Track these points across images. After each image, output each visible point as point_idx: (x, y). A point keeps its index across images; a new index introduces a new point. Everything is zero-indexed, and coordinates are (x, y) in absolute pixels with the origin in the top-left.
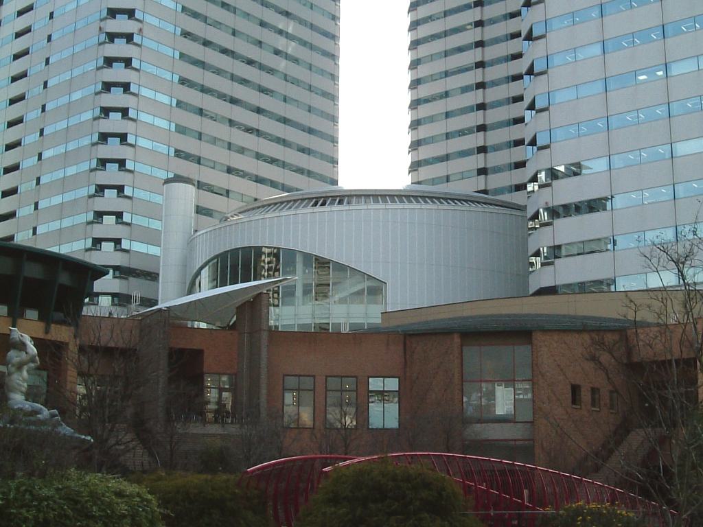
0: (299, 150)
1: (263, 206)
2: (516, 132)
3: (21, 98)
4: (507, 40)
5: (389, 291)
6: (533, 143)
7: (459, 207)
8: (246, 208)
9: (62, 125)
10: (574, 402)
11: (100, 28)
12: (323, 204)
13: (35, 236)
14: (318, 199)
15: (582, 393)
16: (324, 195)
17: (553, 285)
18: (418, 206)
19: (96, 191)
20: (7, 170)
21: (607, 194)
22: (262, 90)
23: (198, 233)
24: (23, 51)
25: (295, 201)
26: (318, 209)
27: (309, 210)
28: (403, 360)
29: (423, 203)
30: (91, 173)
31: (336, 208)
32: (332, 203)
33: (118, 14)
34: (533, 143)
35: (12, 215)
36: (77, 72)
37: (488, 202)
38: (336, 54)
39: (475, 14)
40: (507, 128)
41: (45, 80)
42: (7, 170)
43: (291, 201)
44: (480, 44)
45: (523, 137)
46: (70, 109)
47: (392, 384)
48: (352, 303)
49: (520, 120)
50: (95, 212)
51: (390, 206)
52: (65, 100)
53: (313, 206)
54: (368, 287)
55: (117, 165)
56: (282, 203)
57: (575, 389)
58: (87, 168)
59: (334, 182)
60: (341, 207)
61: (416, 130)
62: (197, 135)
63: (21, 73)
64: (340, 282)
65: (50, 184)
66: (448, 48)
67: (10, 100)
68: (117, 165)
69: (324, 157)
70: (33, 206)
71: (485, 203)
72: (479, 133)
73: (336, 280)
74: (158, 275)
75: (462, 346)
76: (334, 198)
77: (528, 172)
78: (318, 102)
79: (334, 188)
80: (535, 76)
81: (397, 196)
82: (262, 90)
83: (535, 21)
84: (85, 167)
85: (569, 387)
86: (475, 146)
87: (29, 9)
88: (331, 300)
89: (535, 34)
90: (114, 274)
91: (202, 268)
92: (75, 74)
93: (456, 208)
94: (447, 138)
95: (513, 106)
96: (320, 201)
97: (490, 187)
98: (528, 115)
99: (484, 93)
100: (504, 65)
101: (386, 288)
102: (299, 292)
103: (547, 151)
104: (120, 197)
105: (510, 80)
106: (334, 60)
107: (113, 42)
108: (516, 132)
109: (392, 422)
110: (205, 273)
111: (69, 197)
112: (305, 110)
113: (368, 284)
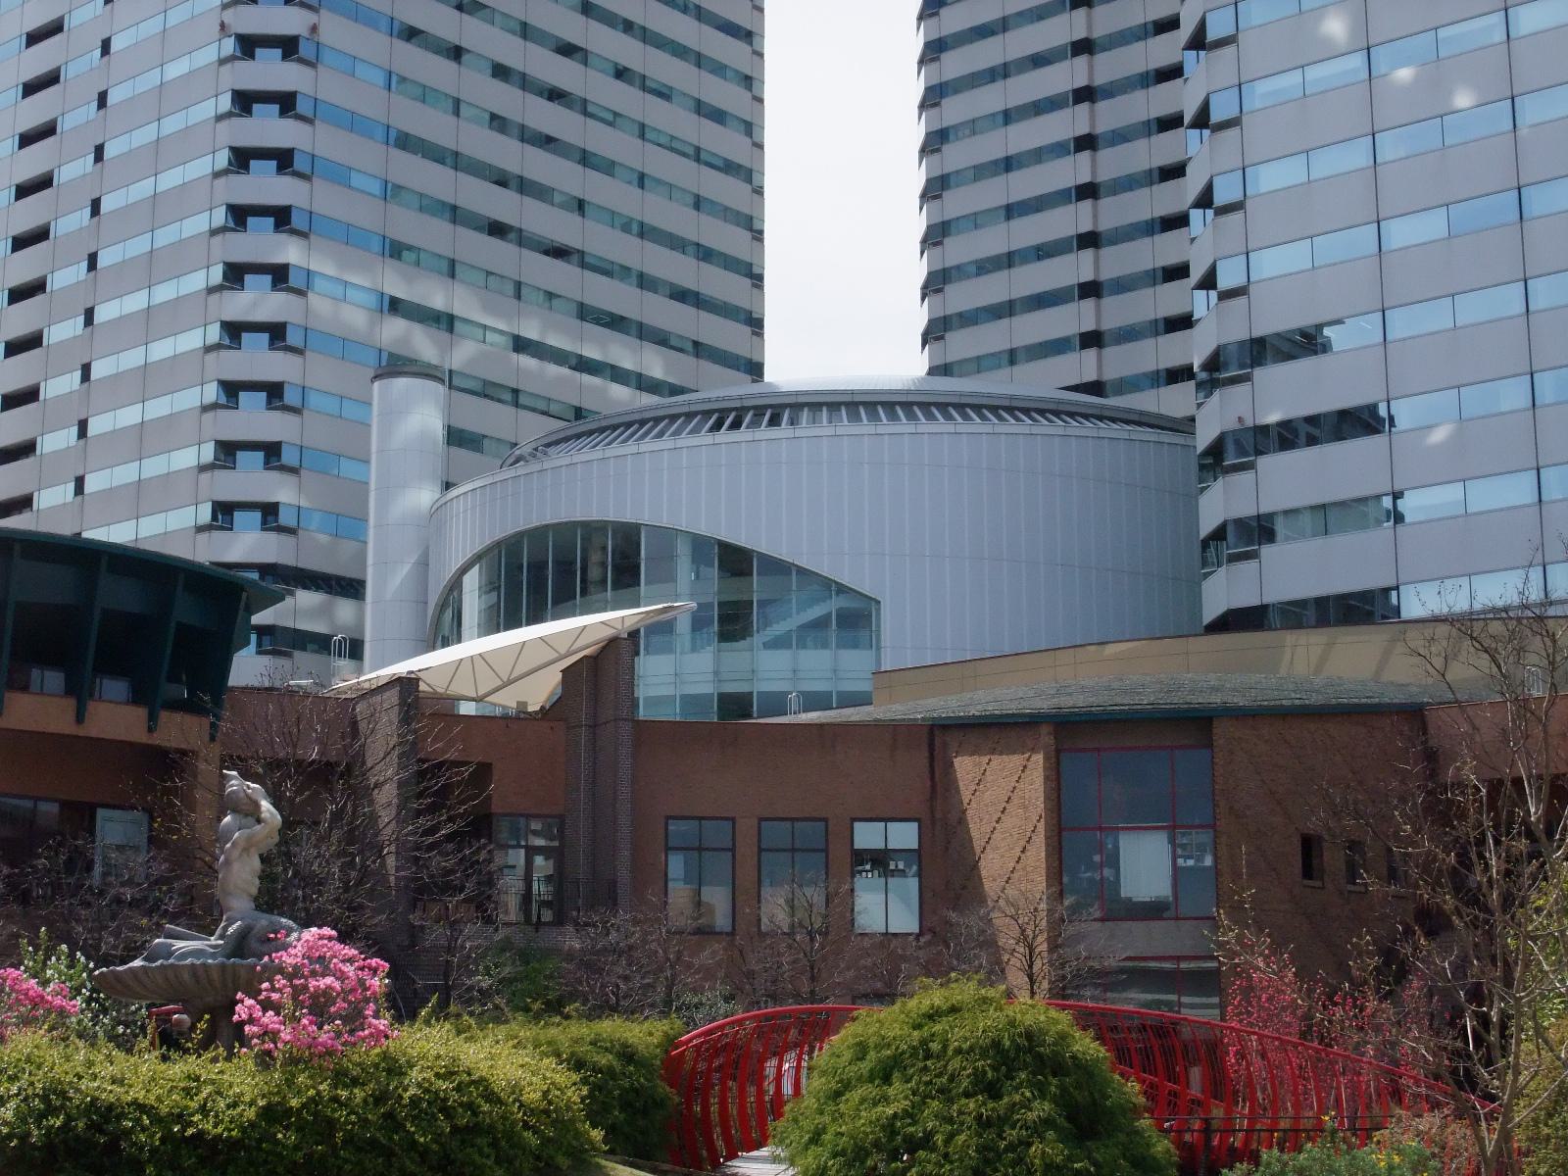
0: (672, 297)
1: (602, 430)
2: (1162, 100)
3: (51, 79)
4: (1152, 184)
5: (888, 622)
6: (1202, 120)
7: (1043, 427)
8: (562, 435)
9: (145, 135)
10: (1308, 872)
11: (223, 26)
12: (736, 425)
13: (79, 498)
14: (723, 413)
15: (1327, 855)
16: (738, 404)
17: (1255, 602)
18: (949, 427)
19: (214, 517)
20: (14, 348)
21: (1390, 582)
22: (585, 159)
23: (454, 492)
24: (46, 74)
25: (673, 418)
26: (724, 436)
27: (705, 438)
28: (929, 783)
29: (960, 420)
30: (216, 182)
31: (765, 433)
32: (755, 424)
33: (261, 46)
34: (1202, 120)
35: (26, 449)
36: (176, 17)
37: (1107, 413)
38: (754, 75)
39: (1071, 26)
40: (1147, 240)
41: (99, 142)
42: (14, 348)
43: (662, 418)
44: (1085, 95)
45: (1185, 259)
46: (162, 100)
47: (904, 836)
48: (804, 647)
49: (1174, 72)
50: (234, 150)
51: (885, 426)
52: (153, 79)
53: (711, 430)
54: (837, 610)
55: (264, 395)
56: (642, 423)
57: (1309, 845)
58: (198, 343)
59: (755, 369)
60: (774, 433)
61: (941, 295)
62: (444, 266)
63: (39, 176)
64: (775, 601)
65: (109, 493)
66: (1013, 103)
67: (15, 239)
68: (264, 395)
69: (730, 168)
70: (81, 319)
71: (1101, 418)
72: (1085, 352)
73: (765, 596)
74: (364, 582)
75: (1058, 751)
76: (759, 411)
77: (1191, 186)
78: (727, 239)
79: (756, 388)
80: (1213, 132)
81: (900, 404)
82: (585, 159)
83: (1218, 171)
84: (196, 281)
85: (1296, 843)
86: (1071, 232)
87: (55, 28)
88: (757, 639)
89: (1212, 35)
90: (259, 644)
91: (464, 570)
92: (159, 243)
93: (1036, 430)
94: (1012, 362)
95: (1167, 340)
96: (728, 418)
97: (1110, 374)
98: (1201, 304)
99: (1094, 161)
100: (1139, 95)
101: (878, 610)
102: (684, 625)
103: (1236, 217)
104: (279, 290)
105: (1154, 127)
106: (749, 179)
107: (252, 56)
108: (1162, 100)
109: (905, 920)
110: (472, 581)
111: (158, 408)
112: (687, 205)
113: (834, 605)
